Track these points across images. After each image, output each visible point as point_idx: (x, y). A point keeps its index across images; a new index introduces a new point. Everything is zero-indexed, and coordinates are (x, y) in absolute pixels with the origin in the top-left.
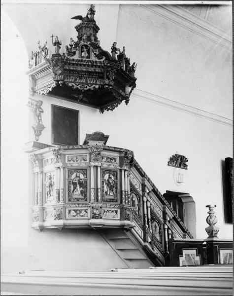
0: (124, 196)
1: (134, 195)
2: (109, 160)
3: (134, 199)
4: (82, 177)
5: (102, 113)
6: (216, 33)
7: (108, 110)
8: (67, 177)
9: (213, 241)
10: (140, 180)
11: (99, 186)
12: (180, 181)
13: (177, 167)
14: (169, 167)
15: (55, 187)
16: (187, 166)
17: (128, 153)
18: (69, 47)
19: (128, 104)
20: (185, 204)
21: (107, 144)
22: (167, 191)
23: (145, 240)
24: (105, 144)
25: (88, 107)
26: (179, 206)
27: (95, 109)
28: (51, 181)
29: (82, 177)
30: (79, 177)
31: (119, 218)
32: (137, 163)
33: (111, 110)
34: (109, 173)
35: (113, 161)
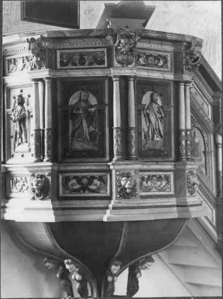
11: (133, 124)
17: (193, 44)
35: (161, 63)
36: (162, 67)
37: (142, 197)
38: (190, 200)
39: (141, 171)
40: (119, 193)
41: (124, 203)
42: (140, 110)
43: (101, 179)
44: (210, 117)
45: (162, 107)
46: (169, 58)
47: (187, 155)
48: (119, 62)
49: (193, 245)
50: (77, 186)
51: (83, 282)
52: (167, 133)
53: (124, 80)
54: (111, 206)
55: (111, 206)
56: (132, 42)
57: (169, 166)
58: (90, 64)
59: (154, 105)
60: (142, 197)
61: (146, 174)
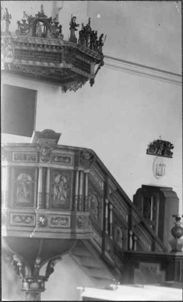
0: (76, 202)
1: (94, 196)
3: (93, 201)
5: (65, 91)
6: (135, 66)
7: (71, 90)
8: (13, 178)
9: (175, 256)
10: (103, 178)
11: (48, 191)
12: (160, 174)
13: (159, 155)
14: (148, 155)
16: (172, 153)
17: (84, 152)
18: (21, 22)
19: (94, 85)
20: (167, 200)
21: (59, 143)
22: (143, 186)
23: (103, 248)
25: (50, 86)
26: (160, 201)
27: (56, 86)
31: (69, 226)
33: (73, 90)
34: (62, 174)
35: (67, 161)
36: (68, 163)
37: (51, 227)
38: (78, 230)
39: (51, 214)
40: (39, 224)
41: (41, 229)
42: (52, 186)
43: (31, 217)
44: (102, 189)
45: (66, 183)
46: (72, 158)
47: (78, 208)
48: (42, 160)
49: (88, 255)
50: (19, 220)
51: (23, 267)
52: (68, 197)
53: (45, 169)
54: (34, 230)
55: (34, 230)
56: (49, 150)
57: (68, 213)
58: (29, 160)
59: (62, 182)
60: (51, 227)
61: (54, 217)
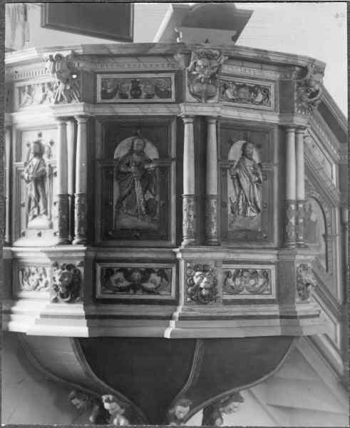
2: (244, 93)
4: (152, 152)
11: (213, 190)
15: (55, 189)
24: (235, 38)
28: (42, 162)
29: (152, 152)
30: (141, 153)
31: (273, 297)
32: (329, 97)
34: (245, 138)
